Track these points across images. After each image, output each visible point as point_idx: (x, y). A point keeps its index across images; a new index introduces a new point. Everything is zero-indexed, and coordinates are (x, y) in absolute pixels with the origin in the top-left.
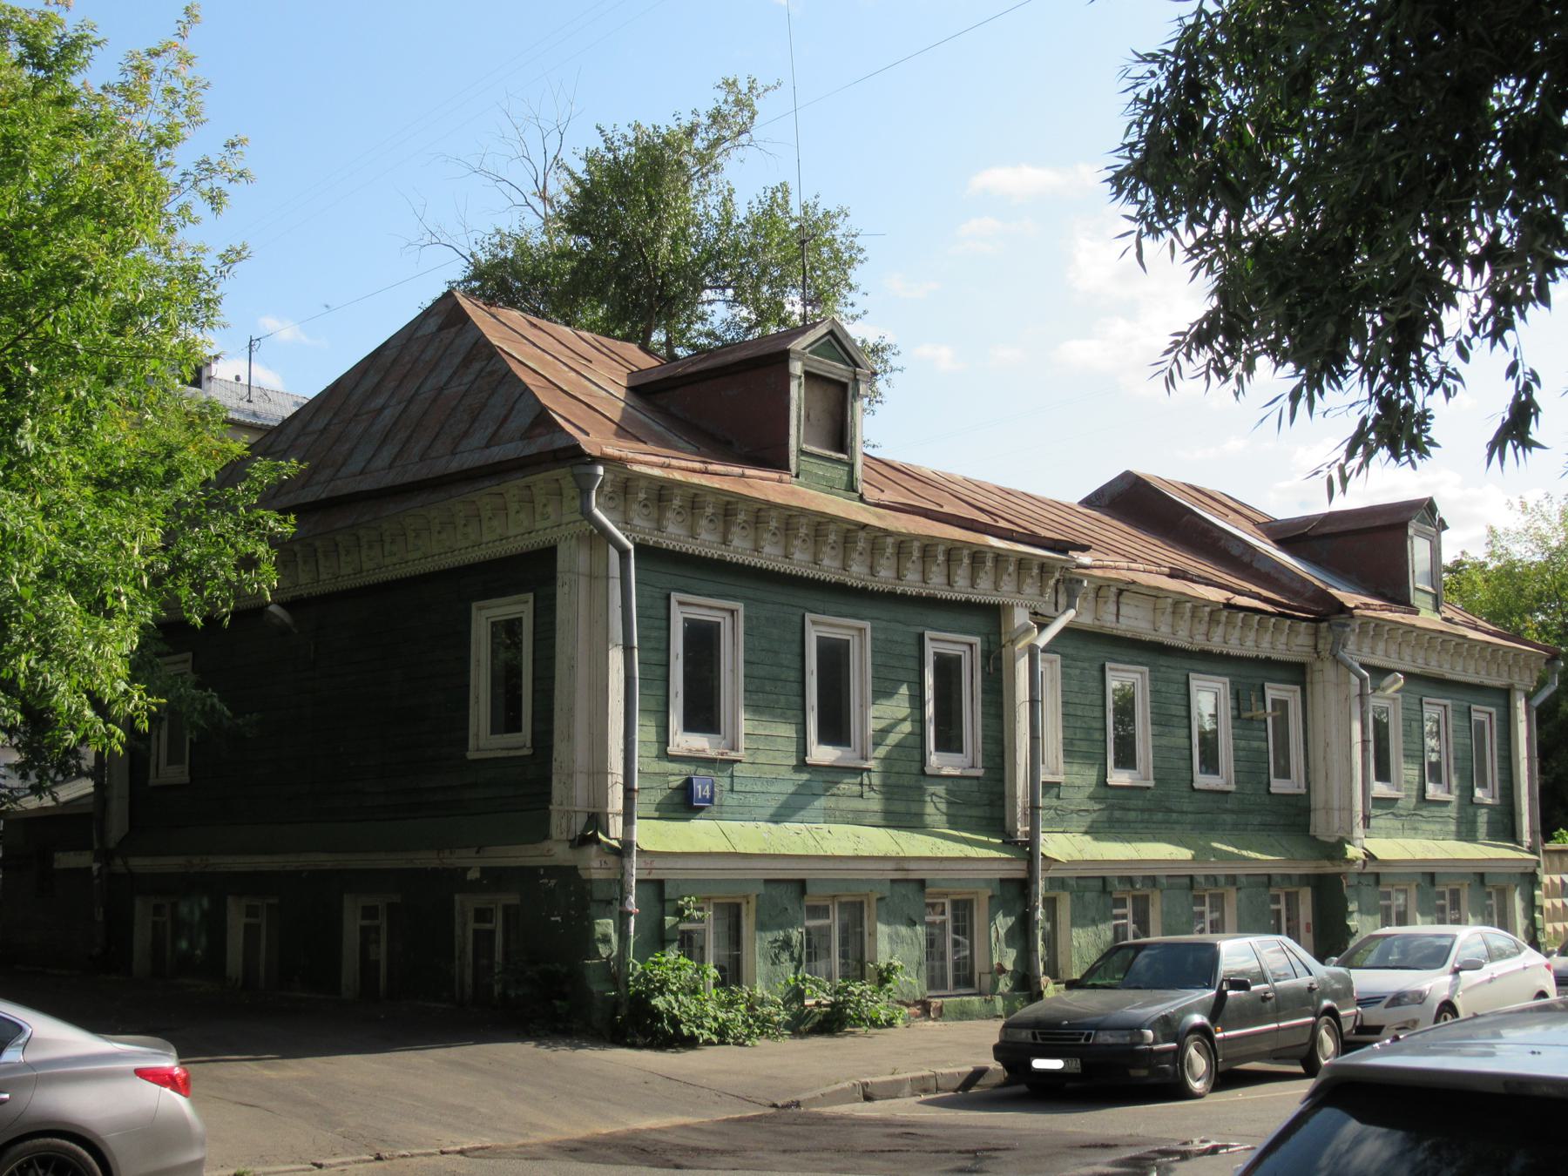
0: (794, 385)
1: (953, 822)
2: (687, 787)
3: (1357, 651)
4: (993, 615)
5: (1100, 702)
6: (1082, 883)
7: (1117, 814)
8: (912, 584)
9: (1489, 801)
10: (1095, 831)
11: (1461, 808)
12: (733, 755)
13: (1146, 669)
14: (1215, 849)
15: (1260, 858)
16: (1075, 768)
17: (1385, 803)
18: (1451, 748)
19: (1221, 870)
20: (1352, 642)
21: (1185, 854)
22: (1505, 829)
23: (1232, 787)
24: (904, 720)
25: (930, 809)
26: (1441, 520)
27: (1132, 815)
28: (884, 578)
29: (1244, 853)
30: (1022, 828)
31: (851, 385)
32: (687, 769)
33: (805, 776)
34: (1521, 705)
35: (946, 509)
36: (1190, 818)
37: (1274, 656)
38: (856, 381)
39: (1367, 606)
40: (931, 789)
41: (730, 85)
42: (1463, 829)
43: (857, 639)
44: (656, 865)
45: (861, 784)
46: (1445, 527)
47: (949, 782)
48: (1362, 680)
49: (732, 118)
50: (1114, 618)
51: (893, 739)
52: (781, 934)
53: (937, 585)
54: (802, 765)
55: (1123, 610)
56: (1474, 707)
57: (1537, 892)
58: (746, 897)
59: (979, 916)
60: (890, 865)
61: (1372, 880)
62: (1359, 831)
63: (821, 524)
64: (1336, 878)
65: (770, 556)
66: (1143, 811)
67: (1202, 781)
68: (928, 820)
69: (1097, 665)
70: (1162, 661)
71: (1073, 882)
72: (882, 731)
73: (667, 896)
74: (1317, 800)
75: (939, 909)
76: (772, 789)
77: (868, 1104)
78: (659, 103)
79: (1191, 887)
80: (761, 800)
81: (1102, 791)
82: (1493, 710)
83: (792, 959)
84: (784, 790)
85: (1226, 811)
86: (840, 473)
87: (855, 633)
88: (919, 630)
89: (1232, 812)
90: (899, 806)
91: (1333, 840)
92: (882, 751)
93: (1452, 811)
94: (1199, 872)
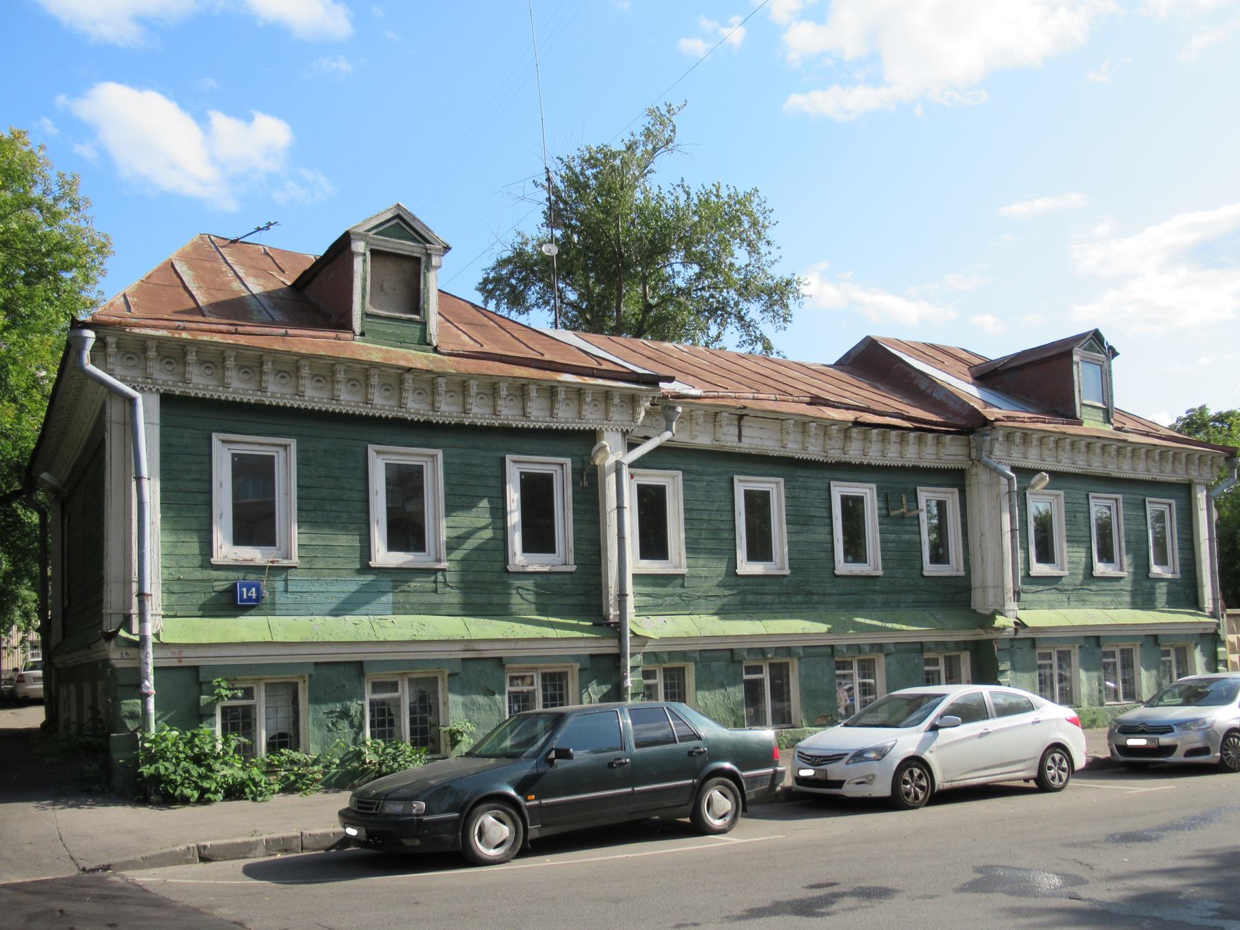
0: (358, 264)
1: (542, 610)
2: (232, 591)
3: (1003, 457)
4: (584, 441)
5: (729, 508)
6: (808, 650)
7: (750, 598)
8: (479, 413)
9: (1169, 576)
10: (724, 612)
11: (1135, 582)
12: (285, 563)
13: (781, 480)
14: (857, 623)
15: (906, 630)
16: (701, 562)
17: (1050, 581)
18: (1122, 533)
19: (865, 640)
20: (998, 451)
21: (822, 628)
22: (1186, 593)
23: (880, 572)
24: (485, 528)
25: (516, 599)
26: (1111, 348)
27: (768, 598)
28: (447, 411)
29: (889, 625)
30: (613, 613)
31: (424, 258)
32: (233, 575)
33: (370, 578)
34: (1201, 496)
35: (547, 357)
36: (833, 599)
37: (923, 464)
38: (429, 256)
39: (1009, 418)
40: (517, 583)
41: (651, 112)
42: (1138, 599)
43: (430, 464)
44: (184, 654)
45: (435, 582)
46: (1115, 354)
47: (538, 578)
48: (1010, 479)
49: (658, 136)
50: (736, 439)
51: (471, 544)
52: (338, 707)
53: (509, 414)
54: (365, 568)
55: (744, 433)
56: (1148, 499)
57: (1220, 649)
58: (303, 677)
59: (573, 685)
60: (461, 647)
61: (1028, 644)
62: (1011, 605)
63: (398, 377)
64: (989, 643)
65: (313, 397)
66: (779, 594)
67: (843, 567)
68: (514, 609)
69: (725, 478)
70: (800, 472)
71: (801, 651)
72: (458, 537)
73: (201, 680)
74: (976, 580)
75: (528, 681)
76: (332, 589)
77: (202, 864)
78: (614, 132)
79: (833, 655)
80: (320, 598)
81: (733, 580)
82: (1173, 502)
83: (352, 725)
84: (346, 589)
85: (875, 592)
86: (416, 331)
87: (558, 468)
88: (501, 454)
89: (882, 592)
90: (480, 599)
91: (988, 612)
92: (458, 555)
93: (1127, 586)
94: (839, 641)
